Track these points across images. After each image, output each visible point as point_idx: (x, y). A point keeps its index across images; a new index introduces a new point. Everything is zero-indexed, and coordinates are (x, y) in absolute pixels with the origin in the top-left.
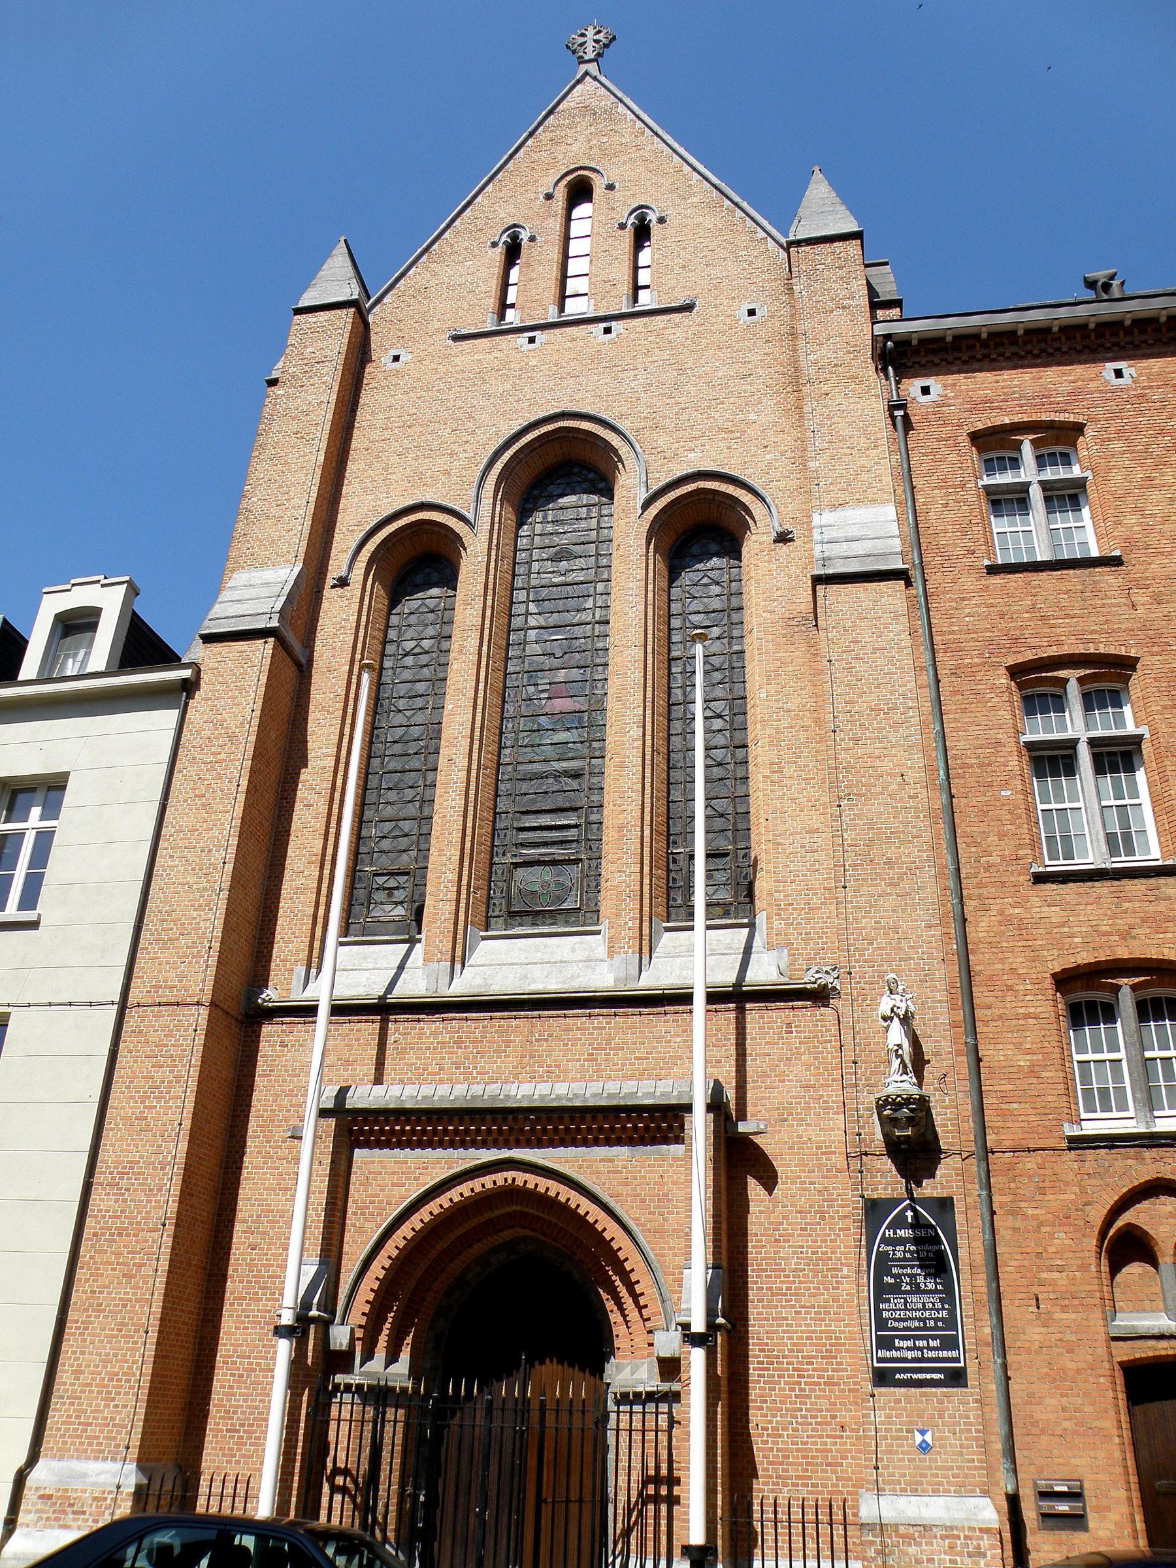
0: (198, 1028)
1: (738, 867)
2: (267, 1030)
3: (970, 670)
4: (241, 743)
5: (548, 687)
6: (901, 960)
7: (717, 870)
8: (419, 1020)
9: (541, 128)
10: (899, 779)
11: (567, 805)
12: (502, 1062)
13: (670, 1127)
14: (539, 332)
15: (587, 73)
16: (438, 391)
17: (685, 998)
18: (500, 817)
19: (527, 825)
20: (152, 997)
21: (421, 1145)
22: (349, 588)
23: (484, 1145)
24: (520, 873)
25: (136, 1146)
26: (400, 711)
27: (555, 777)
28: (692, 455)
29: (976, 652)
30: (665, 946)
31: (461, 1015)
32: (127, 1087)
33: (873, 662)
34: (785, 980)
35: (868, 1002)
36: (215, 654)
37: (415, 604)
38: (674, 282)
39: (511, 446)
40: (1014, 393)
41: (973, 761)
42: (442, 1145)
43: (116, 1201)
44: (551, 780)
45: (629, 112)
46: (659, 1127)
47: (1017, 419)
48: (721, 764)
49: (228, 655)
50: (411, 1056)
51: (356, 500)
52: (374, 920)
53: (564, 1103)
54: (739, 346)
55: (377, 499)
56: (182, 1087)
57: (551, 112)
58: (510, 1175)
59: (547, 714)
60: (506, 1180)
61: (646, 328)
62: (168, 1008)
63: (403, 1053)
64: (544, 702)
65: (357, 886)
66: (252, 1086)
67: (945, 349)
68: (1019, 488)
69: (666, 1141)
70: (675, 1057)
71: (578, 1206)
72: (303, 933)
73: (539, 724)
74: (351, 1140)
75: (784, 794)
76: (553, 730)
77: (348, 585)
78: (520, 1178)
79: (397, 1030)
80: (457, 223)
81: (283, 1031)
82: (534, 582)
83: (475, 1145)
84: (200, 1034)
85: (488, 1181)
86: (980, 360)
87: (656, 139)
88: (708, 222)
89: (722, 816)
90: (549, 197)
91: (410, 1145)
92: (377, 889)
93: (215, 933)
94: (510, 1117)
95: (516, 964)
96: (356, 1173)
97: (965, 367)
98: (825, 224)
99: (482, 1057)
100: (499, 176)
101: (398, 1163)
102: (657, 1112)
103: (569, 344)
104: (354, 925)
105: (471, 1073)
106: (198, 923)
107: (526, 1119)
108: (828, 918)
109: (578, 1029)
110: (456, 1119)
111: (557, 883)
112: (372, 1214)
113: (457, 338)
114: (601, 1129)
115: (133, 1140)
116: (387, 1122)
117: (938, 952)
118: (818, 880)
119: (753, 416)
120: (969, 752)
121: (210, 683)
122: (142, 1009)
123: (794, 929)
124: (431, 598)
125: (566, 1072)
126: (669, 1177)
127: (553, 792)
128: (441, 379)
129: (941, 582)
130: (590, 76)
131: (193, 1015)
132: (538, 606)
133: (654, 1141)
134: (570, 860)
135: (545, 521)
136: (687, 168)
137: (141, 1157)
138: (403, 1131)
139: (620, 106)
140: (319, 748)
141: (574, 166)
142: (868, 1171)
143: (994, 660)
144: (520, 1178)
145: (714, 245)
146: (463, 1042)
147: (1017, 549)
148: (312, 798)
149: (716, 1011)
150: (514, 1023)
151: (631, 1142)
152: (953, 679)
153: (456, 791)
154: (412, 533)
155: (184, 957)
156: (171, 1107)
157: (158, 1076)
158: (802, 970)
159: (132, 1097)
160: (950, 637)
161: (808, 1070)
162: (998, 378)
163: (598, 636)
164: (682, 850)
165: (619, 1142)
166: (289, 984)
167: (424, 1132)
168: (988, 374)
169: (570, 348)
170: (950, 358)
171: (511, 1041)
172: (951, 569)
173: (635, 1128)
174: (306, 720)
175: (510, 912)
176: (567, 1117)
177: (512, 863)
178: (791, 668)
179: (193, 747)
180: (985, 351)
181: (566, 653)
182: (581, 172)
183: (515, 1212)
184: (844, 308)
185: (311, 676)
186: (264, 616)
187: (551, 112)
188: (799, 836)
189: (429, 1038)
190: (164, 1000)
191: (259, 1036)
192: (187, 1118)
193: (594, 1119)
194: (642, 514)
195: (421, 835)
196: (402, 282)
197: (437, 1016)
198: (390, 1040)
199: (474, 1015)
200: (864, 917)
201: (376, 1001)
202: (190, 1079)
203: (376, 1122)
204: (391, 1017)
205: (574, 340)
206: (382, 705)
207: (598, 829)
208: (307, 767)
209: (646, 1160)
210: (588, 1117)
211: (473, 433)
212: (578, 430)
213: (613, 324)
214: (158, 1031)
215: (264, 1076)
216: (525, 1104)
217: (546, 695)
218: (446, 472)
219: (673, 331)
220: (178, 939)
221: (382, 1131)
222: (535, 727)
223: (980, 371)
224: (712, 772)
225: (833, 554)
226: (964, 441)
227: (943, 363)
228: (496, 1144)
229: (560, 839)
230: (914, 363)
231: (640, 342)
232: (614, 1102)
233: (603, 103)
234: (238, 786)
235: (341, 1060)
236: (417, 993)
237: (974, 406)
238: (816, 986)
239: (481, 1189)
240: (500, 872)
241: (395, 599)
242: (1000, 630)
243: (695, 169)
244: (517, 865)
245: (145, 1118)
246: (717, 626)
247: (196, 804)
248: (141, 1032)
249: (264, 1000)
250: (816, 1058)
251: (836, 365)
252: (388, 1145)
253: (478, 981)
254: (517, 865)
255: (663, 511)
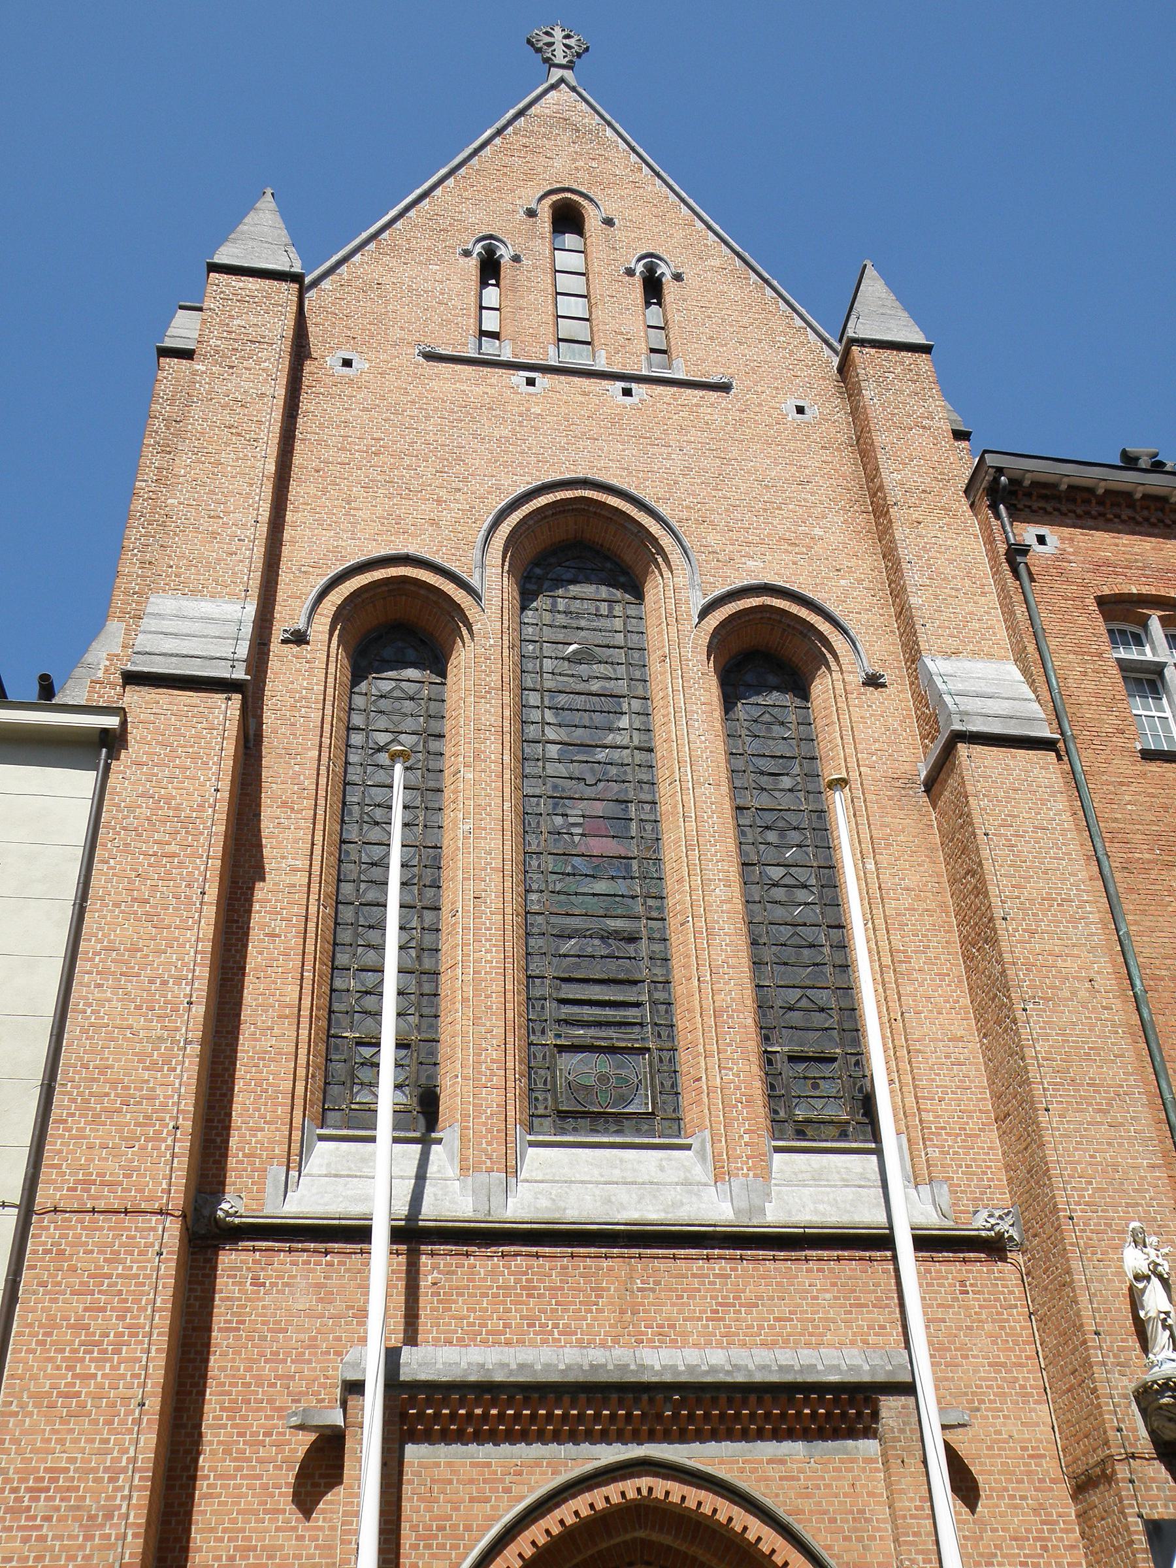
0: (165, 1251)
1: (850, 1076)
2: (228, 1259)
3: (1142, 866)
4: (202, 834)
5: (581, 820)
6: (1128, 1205)
7: (824, 1078)
8: (467, 1255)
9: (511, 129)
10: (1088, 985)
11: (622, 976)
12: (594, 1319)
13: (859, 1414)
14: (540, 375)
15: (562, 80)
16: (412, 417)
17: (360, 1234)
18: (534, 983)
19: (571, 996)
20: (80, 1198)
21: (511, 1437)
22: (309, 648)
23: (605, 1437)
24: (568, 1062)
25: (61, 1442)
26: (377, 823)
27: (602, 938)
28: (750, 563)
29: (1146, 847)
30: (781, 1171)
31: (529, 1249)
32: (42, 1343)
33: (1035, 842)
34: (949, 1223)
35: (1099, 1256)
36: (147, 703)
37: (386, 686)
38: (702, 354)
39: (518, 507)
40: (1136, 561)
41: (1164, 973)
42: (541, 1437)
43: (26, 1540)
44: (597, 942)
45: (620, 140)
46: (844, 1414)
47: (1145, 590)
48: (814, 946)
49: (169, 707)
50: (460, 1305)
51: (308, 532)
52: (362, 1107)
53: (722, 1378)
54: (791, 446)
55: (337, 537)
56: (142, 1343)
57: (521, 113)
58: (644, 1482)
59: (583, 855)
60: (639, 1490)
61: (676, 400)
62: (109, 1216)
63: (447, 1301)
64: (577, 838)
65: (334, 1057)
66: (208, 1345)
67: (1058, 498)
68: (1153, 668)
69: (852, 1434)
70: (827, 1320)
71: (745, 1529)
72: (278, 1117)
73: (573, 866)
74: (401, 1429)
75: (916, 990)
76: (593, 876)
77: (308, 643)
78: (661, 1487)
79: (435, 1267)
80: (412, 213)
81: (255, 1262)
82: (548, 684)
83: (591, 1437)
84: (168, 1260)
85: (614, 1491)
86: (1095, 518)
87: (658, 181)
88: (733, 291)
89: (822, 1010)
90: (531, 213)
91: (494, 1437)
92: (362, 1064)
93: (182, 1107)
94: (645, 1397)
95: (590, 1182)
96: (411, 1482)
97: (1079, 522)
98: (888, 329)
99: (565, 1311)
100: (463, 171)
101: (476, 1465)
102: (845, 1393)
103: (581, 398)
104: (333, 1113)
105: (551, 1333)
106: (153, 1089)
107: (668, 1399)
108: (990, 1148)
109: (694, 1276)
110: (567, 1399)
111: (619, 1078)
112: (443, 1546)
113: (431, 357)
114: (768, 1416)
115: (54, 1432)
116: (462, 1403)
117: (1168, 1198)
118: (971, 1100)
119: (818, 532)
120: (1157, 962)
121: (143, 741)
122: (60, 1216)
123: (952, 1160)
124: (409, 681)
125: (685, 1334)
126: (862, 1486)
127: (602, 957)
128: (413, 402)
129: (1093, 760)
130: (568, 85)
131: (154, 1229)
132: (556, 715)
133: (836, 1435)
134: (633, 1048)
135: (553, 610)
136: (700, 225)
137: (72, 1460)
138: (485, 1416)
139: (608, 130)
140: (283, 858)
141: (558, 186)
142: (1140, 1479)
143: (1166, 858)
144: (661, 1487)
145: (745, 321)
146: (535, 1288)
147: (1156, 736)
148: (278, 926)
149: (871, 1261)
150: (605, 1264)
151: (806, 1435)
152: (1126, 875)
153: (490, 940)
154: (389, 591)
155: (132, 1139)
156: (123, 1377)
157: (96, 1324)
158: (968, 1212)
159: (49, 1360)
160: (1114, 825)
161: (994, 1343)
162: (1117, 541)
163: (639, 766)
164: (779, 1049)
165: (791, 1435)
166: (261, 1191)
167: (517, 1417)
168: (1106, 535)
169: (582, 403)
170: (1064, 509)
171: (603, 1289)
172: (1101, 747)
173: (814, 1414)
174: (258, 815)
175: (559, 1112)
176: (723, 1396)
177: (555, 1045)
178: (902, 838)
179: (124, 829)
180: (1101, 509)
181: (600, 780)
182: (569, 195)
183: (635, 1540)
184: (924, 427)
185: (260, 758)
186: (223, 663)
187: (521, 113)
188: (941, 1044)
189: (485, 1280)
190: (101, 1205)
191: (215, 1268)
192: (154, 1394)
193: (760, 1402)
194: (699, 623)
195: (422, 995)
196: (344, 268)
197: (493, 1249)
198: (425, 1282)
199: (547, 1249)
200: (1076, 1149)
201: (403, 1223)
202: (155, 1332)
203: (445, 1402)
204: (423, 1247)
205: (585, 394)
206: (350, 813)
207: (667, 1012)
208: (263, 880)
209: (829, 1462)
210: (753, 1398)
211: (465, 480)
212: (604, 505)
213: (634, 386)
214: (92, 1252)
215: (228, 1330)
216: (668, 1378)
217: (579, 830)
218: (433, 522)
219: (709, 410)
220: (119, 1111)
221: (453, 1416)
222: (569, 870)
223: (1097, 529)
224: (801, 954)
225: (969, 708)
226: (1090, 601)
227: (1055, 513)
228: (621, 1438)
229: (618, 1019)
230: (1025, 506)
231: (671, 415)
232: (789, 1378)
233: (586, 120)
234: (203, 893)
235: (352, 1308)
236: (460, 1215)
237: (1098, 567)
238: (993, 1233)
239: (605, 1505)
240: (540, 1056)
241: (358, 674)
242: (1167, 825)
243: (710, 228)
244: (561, 1049)
245: (77, 1395)
246: (787, 774)
247: (135, 913)
248: (61, 1252)
249: (228, 1214)
250: (1002, 1328)
251: (924, 491)
252: (460, 1437)
253: (544, 1203)
254: (561, 1049)
255: (723, 624)
